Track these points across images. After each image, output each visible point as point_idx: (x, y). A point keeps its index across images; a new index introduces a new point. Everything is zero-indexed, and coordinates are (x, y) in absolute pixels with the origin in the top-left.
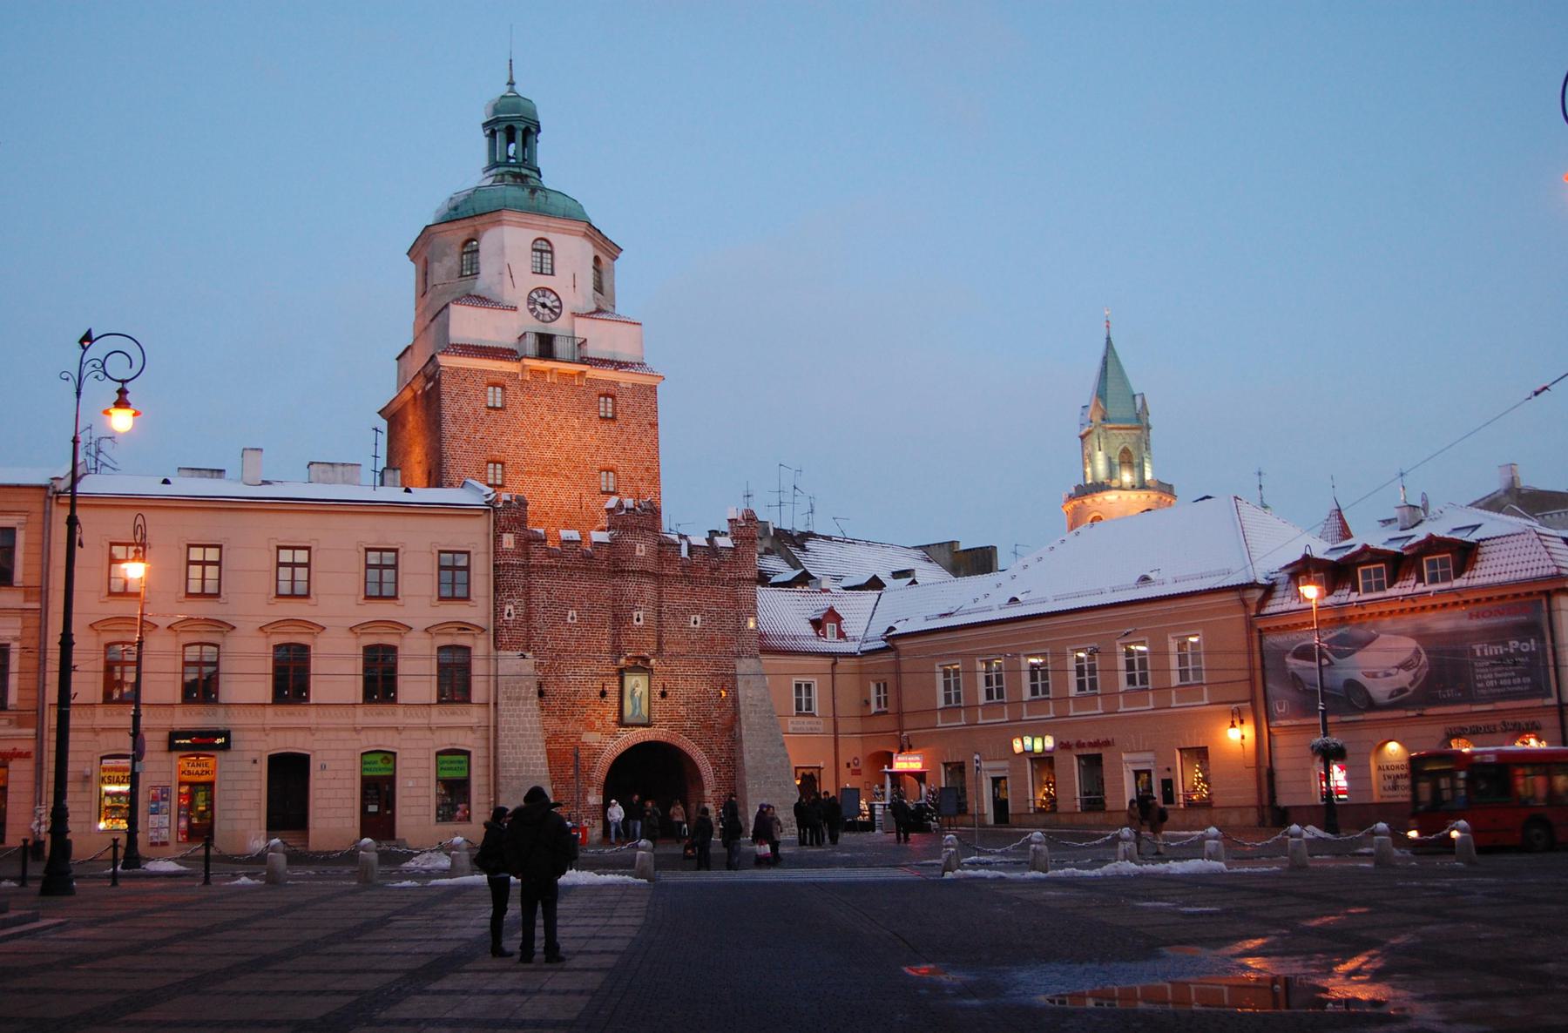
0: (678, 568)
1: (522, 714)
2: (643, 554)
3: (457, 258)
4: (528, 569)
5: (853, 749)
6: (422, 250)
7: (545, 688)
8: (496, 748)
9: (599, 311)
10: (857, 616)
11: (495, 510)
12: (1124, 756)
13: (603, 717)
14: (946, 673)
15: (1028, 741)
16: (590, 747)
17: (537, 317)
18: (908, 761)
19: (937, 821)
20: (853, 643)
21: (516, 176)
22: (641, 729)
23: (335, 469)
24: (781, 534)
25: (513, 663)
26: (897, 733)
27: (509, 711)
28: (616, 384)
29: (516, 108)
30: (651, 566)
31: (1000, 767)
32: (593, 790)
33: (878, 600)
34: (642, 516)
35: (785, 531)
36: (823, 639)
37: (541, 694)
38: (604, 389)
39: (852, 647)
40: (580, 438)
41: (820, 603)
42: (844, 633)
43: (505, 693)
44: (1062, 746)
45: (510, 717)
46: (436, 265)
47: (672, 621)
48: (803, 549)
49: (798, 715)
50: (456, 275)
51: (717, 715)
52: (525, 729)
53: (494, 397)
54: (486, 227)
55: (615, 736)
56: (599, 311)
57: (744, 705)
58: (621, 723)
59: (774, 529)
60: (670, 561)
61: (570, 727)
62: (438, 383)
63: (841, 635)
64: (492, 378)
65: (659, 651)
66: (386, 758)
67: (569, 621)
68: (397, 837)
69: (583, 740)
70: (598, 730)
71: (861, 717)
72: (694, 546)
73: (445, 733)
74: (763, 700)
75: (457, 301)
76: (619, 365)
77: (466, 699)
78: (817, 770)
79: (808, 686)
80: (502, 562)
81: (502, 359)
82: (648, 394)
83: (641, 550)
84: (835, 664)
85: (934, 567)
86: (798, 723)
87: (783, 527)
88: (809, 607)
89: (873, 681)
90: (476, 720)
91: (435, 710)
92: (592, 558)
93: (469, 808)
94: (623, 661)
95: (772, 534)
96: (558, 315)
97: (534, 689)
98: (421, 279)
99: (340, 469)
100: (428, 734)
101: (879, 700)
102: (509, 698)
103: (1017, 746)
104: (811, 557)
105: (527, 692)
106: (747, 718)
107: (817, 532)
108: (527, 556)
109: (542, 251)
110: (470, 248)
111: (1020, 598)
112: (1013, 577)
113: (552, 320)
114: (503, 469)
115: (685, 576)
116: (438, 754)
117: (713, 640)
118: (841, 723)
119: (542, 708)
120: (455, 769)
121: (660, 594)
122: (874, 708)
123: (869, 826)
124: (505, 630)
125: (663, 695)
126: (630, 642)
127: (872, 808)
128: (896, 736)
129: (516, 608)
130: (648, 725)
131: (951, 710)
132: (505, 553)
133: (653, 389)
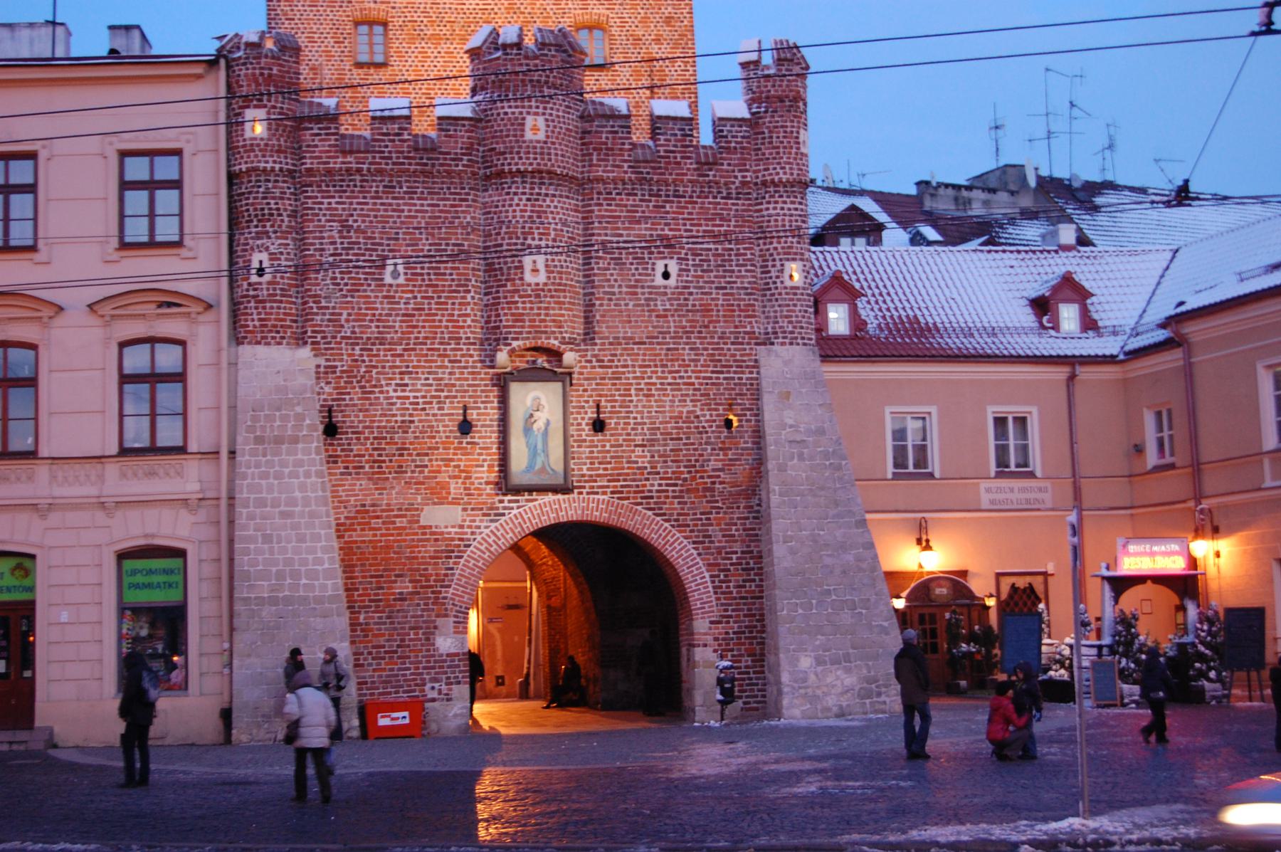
0: (626, 165)
1: (287, 471)
2: (541, 136)
4: (299, 179)
7: (338, 417)
10: (1126, 290)
16: (437, 536)
18: (1152, 554)
19: (1219, 679)
20: (1112, 338)
22: (550, 497)
23: (17, 33)
24: (1050, 186)
26: (1191, 504)
27: (258, 466)
30: (564, 159)
33: (1171, 261)
34: (536, 57)
35: (1060, 181)
36: (1052, 332)
37: (331, 430)
42: (1095, 322)
43: (251, 429)
45: (261, 478)
47: (614, 273)
49: (999, 475)
51: (720, 465)
52: (292, 502)
55: (494, 514)
57: (776, 443)
58: (505, 484)
59: (1039, 178)
60: (606, 151)
61: (394, 495)
63: (1089, 324)
66: (19, 567)
67: (388, 279)
68: (38, 723)
69: (423, 523)
70: (455, 502)
71: (1130, 476)
72: (659, 117)
73: (134, 514)
74: (821, 432)
78: (1040, 579)
79: (1021, 422)
80: (244, 167)
83: (536, 128)
84: (1072, 377)
86: (999, 490)
87: (1057, 174)
88: (1030, 278)
89: (1148, 407)
90: (196, 487)
92: (433, 150)
97: (314, 422)
99: (26, 33)
100: (100, 516)
101: (1160, 442)
105: (298, 427)
106: (782, 468)
108: (298, 154)
114: (385, 34)
115: (642, 181)
116: (122, 556)
117: (706, 310)
118: (1087, 486)
119: (332, 460)
120: (158, 586)
121: (587, 223)
124: (252, 304)
125: (599, 426)
126: (518, 318)
128: (1189, 509)
129: (273, 257)
130: (565, 489)
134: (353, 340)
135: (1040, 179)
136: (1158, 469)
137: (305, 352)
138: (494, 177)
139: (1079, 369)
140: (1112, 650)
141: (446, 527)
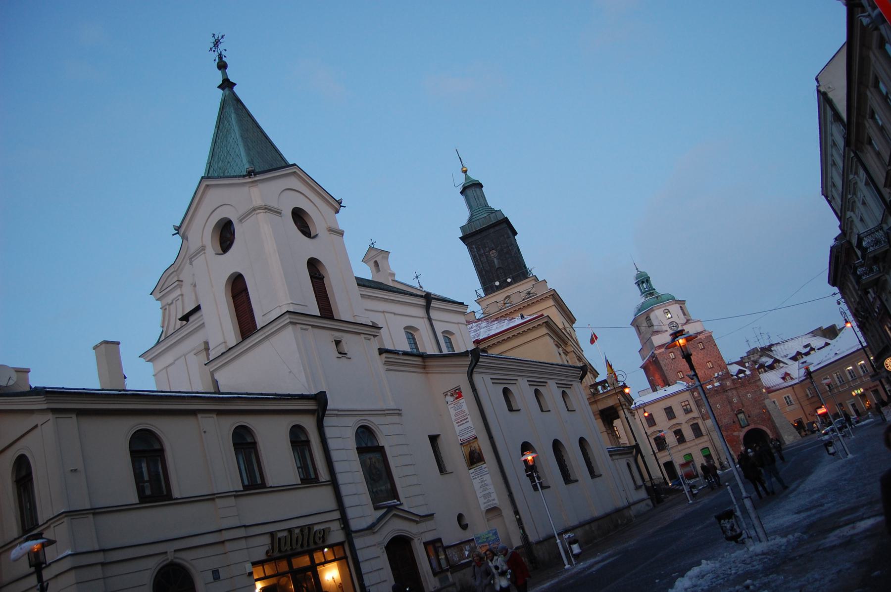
6: (635, 323)
12: (847, 402)
13: (736, 427)
15: (859, 392)
21: (650, 294)
24: (763, 349)
32: (742, 446)
35: (763, 347)
39: (796, 381)
40: (698, 357)
44: (866, 390)
48: (771, 351)
49: (789, 406)
54: (650, 313)
62: (657, 358)
63: (792, 379)
75: (652, 335)
77: (701, 435)
79: (788, 397)
82: (710, 338)
83: (728, 383)
91: (696, 440)
93: (714, 461)
94: (735, 412)
95: (759, 350)
103: (854, 394)
107: (774, 343)
109: (667, 313)
110: (648, 319)
111: (837, 353)
112: (834, 346)
118: (801, 403)
121: (738, 392)
122: (810, 396)
125: (749, 417)
130: (749, 425)
132: (696, 397)
133: (711, 336)
136: (812, 397)
138: (726, 391)
139: (794, 386)
141: (539, 478)
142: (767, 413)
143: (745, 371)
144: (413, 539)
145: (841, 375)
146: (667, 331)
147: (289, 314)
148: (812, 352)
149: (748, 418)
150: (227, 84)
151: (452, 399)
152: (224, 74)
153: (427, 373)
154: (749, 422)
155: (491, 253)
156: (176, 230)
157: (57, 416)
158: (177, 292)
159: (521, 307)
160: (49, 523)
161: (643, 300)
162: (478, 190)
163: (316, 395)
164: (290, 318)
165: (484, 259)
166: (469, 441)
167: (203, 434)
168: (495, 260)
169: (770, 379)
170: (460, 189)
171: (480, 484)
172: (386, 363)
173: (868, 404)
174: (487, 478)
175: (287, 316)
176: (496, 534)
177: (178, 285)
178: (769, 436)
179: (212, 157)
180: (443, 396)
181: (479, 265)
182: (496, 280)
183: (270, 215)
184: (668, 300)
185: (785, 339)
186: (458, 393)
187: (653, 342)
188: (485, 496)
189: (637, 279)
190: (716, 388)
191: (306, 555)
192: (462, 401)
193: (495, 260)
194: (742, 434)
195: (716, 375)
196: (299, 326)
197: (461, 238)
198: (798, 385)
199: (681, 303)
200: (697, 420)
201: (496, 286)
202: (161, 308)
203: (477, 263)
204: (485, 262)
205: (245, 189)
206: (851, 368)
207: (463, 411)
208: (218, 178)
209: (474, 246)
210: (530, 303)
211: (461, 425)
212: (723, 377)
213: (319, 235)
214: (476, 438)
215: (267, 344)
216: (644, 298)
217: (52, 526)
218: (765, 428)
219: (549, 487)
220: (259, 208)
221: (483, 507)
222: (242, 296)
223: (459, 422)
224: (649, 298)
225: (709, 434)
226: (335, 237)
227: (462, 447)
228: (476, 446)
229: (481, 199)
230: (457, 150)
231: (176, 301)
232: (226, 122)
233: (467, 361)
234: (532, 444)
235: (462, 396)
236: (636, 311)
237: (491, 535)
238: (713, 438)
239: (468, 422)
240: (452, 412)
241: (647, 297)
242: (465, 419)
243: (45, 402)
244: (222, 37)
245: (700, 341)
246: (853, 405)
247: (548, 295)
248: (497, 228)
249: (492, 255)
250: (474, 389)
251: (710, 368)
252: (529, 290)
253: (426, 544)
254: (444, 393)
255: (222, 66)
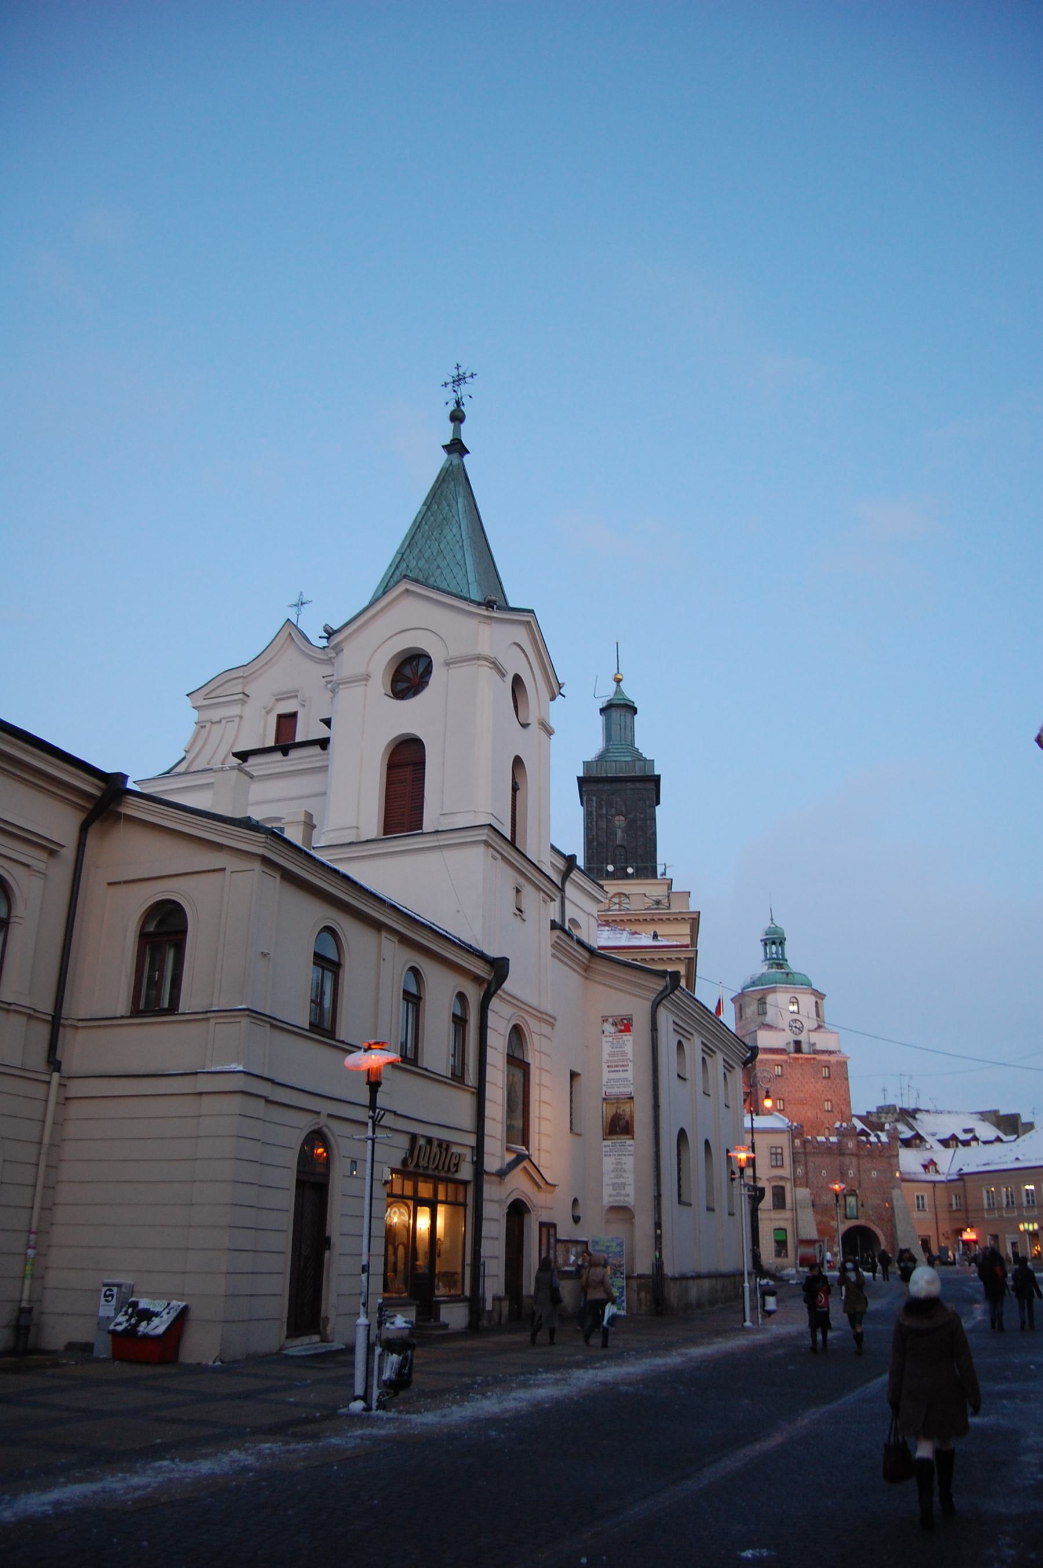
3: (756, 1006)
5: (946, 1227)
8: (797, 1229)
9: (819, 1027)
11: (791, 1129)
12: (1007, 1236)
14: (988, 1192)
15: (1026, 1225)
17: (793, 1032)
25: (803, 1193)
28: (829, 1061)
29: (775, 933)
31: (1014, 1237)
37: (813, 1206)
38: (824, 1064)
40: (815, 1087)
41: (926, 1156)
46: (747, 1009)
48: (915, 1118)
49: (918, 1210)
50: (756, 1014)
53: (778, 1070)
54: (769, 993)
55: (843, 1223)
56: (819, 1027)
58: (846, 1217)
63: (937, 1172)
64: (777, 1063)
65: (860, 1186)
75: (760, 1028)
76: (831, 1053)
81: (781, 1054)
82: (843, 1064)
83: (851, 1144)
85: (987, 1124)
96: (802, 1031)
97: (810, 1205)
98: (738, 1011)
101: (957, 1204)
102: (801, 1207)
103: (1021, 1227)
104: (919, 1122)
107: (921, 1108)
108: (805, 1148)
110: (762, 1002)
111: (1020, 1158)
113: (799, 1034)
116: (775, 1230)
118: (938, 1215)
121: (859, 1163)
123: (953, 1263)
125: (862, 1206)
127: (954, 1256)
130: (857, 1218)
131: (991, 1209)
132: (796, 1147)
133: (845, 1063)
134: (817, 1187)
135: (900, 1109)
136: (957, 1210)
137: (808, 1189)
138: (842, 1154)
139: (937, 1185)
140: (962, 1254)
142: (890, 1209)
143: (870, 1135)
144: (530, 1211)
145: (1014, 1193)
146: (784, 1030)
147: (489, 830)
148: (973, 1143)
149: (860, 1206)
150: (456, 447)
151: (612, 1029)
152: (457, 431)
153: (587, 978)
154: (860, 1214)
155: (617, 818)
156: (326, 631)
157: (267, 871)
158: (235, 710)
159: (641, 918)
160: (209, 1015)
161: (764, 969)
162: (629, 715)
163: (495, 959)
164: (488, 835)
165: (603, 824)
166: (618, 1098)
167: (382, 961)
168: (619, 832)
169: (909, 1160)
170: (602, 703)
171: (615, 1166)
172: (556, 945)
173: (1037, 1251)
174: (629, 1162)
175: (486, 831)
176: (620, 1245)
177: (240, 700)
178: (880, 1245)
179: (408, 546)
180: (600, 1020)
181: (591, 829)
182: (609, 861)
183: (494, 673)
184: (802, 985)
185: (940, 1108)
186: (625, 1025)
187: (758, 1038)
188: (615, 1186)
189: (767, 935)
190: (829, 1145)
191: (430, 1183)
192: (627, 1038)
193: (619, 832)
194: (843, 1227)
195: (837, 1125)
196: (491, 850)
197: (579, 778)
198: (942, 1185)
199: (819, 996)
200: (786, 1182)
201: (607, 870)
202: (196, 723)
203: (589, 825)
204: (603, 828)
205: (473, 623)
206: (1032, 1187)
207: (624, 1054)
208: (433, 589)
209: (594, 799)
210: (656, 917)
211: (614, 1071)
212: (846, 1133)
213: (530, 726)
214: (632, 1098)
215: (436, 856)
216: (767, 967)
217: (212, 1022)
218: (879, 1232)
219: (690, 1205)
220: (486, 659)
221: (607, 1200)
222: (406, 772)
223: (612, 1066)
224: (774, 970)
225: (794, 1210)
226: (543, 734)
227: (605, 1105)
228: (628, 1110)
229: (628, 732)
230: (617, 644)
231: (227, 722)
232: (444, 504)
233: (659, 985)
234: (688, 1134)
235: (630, 1031)
236: (749, 983)
237: (614, 1244)
238: (799, 1219)
239: (627, 1071)
240: (606, 1049)
241: (772, 968)
242: (623, 1066)
243: (263, 845)
244: (472, 376)
245: (828, 1064)
246: (1014, 1244)
247: (686, 916)
248: (639, 785)
249: (616, 822)
250: (654, 1028)
251: (826, 1111)
252: (660, 898)
253: (542, 1225)
254: (602, 1017)
255: (457, 417)
